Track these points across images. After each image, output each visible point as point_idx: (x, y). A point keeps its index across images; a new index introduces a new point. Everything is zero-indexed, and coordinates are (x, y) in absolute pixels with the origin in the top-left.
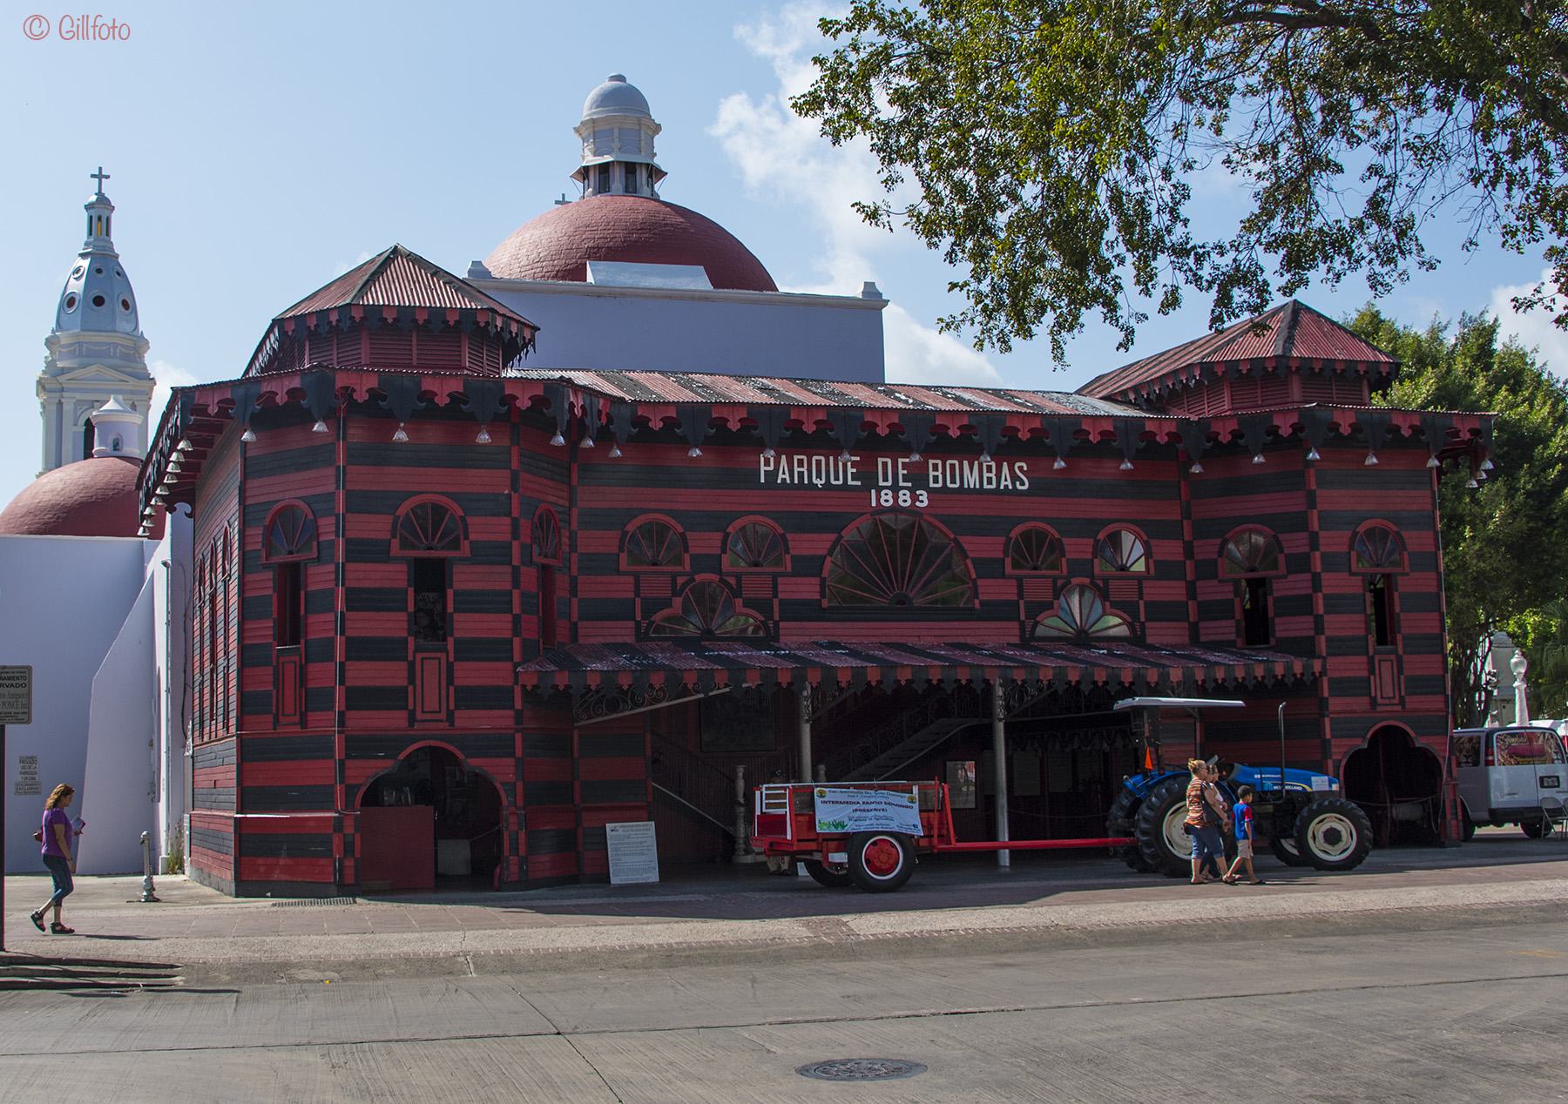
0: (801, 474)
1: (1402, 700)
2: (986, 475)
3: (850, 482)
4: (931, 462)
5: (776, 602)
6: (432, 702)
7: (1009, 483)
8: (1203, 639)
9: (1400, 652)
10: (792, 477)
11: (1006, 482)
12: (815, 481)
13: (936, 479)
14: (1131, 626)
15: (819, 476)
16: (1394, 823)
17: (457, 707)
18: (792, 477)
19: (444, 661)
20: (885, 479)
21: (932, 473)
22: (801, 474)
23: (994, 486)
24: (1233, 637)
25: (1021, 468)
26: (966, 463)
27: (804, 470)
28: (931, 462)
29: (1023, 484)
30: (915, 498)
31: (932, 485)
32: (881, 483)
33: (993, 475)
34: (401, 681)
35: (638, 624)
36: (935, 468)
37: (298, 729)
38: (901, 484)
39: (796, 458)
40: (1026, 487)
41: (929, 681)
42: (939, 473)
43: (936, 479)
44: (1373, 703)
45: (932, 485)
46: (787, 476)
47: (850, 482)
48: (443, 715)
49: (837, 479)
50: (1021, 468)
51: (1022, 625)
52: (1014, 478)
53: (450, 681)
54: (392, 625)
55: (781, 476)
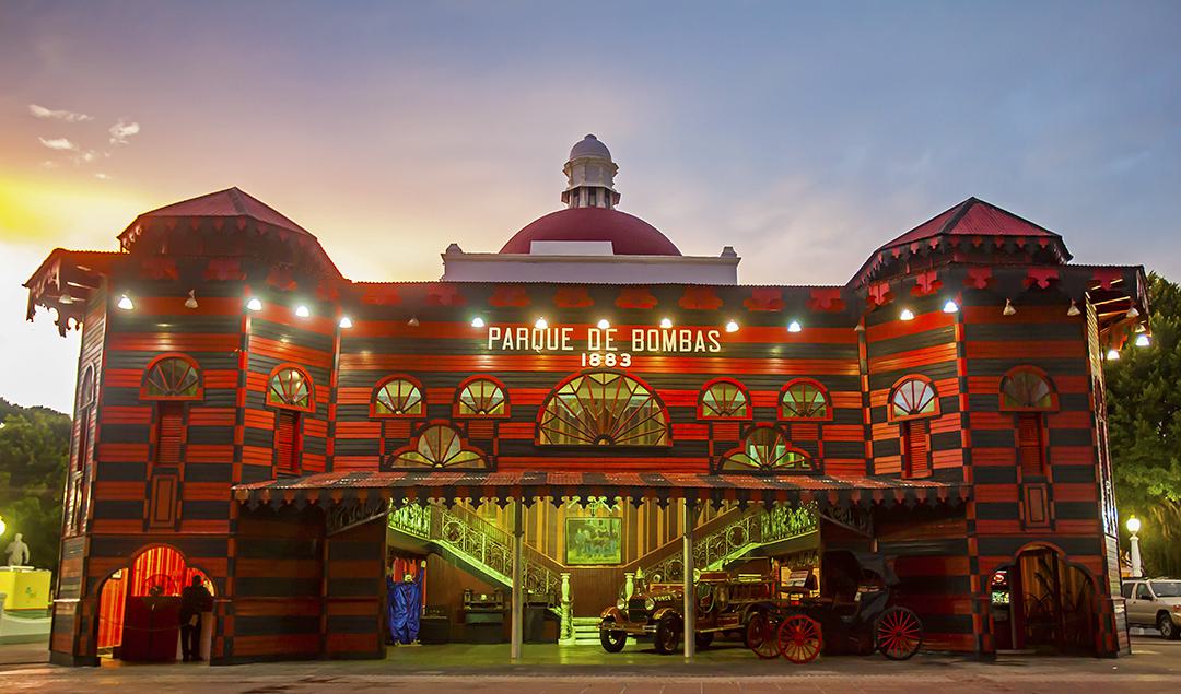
0: (522, 342)
1: (1052, 522)
2: (682, 341)
3: (564, 348)
4: (634, 331)
5: (496, 441)
6: (163, 514)
8: (877, 473)
9: (1051, 481)
11: (700, 346)
13: (638, 345)
14: (485, 459)
15: (537, 344)
16: (995, 623)
17: (1057, 517)
19: (175, 480)
21: (635, 340)
22: (522, 342)
23: (689, 349)
24: (899, 470)
25: (713, 335)
27: (526, 339)
28: (634, 331)
30: (619, 360)
31: (634, 349)
32: (590, 348)
33: (689, 341)
34: (1012, 499)
35: (382, 458)
36: (638, 335)
37: (1050, 531)
39: (519, 330)
41: (261, 502)
42: (641, 340)
43: (638, 345)
44: (1023, 525)
45: (634, 349)
46: (511, 344)
47: (564, 348)
48: (171, 524)
49: (553, 345)
50: (713, 335)
51: (711, 459)
52: (707, 342)
53: (180, 494)
54: (1003, 456)
55: (505, 344)
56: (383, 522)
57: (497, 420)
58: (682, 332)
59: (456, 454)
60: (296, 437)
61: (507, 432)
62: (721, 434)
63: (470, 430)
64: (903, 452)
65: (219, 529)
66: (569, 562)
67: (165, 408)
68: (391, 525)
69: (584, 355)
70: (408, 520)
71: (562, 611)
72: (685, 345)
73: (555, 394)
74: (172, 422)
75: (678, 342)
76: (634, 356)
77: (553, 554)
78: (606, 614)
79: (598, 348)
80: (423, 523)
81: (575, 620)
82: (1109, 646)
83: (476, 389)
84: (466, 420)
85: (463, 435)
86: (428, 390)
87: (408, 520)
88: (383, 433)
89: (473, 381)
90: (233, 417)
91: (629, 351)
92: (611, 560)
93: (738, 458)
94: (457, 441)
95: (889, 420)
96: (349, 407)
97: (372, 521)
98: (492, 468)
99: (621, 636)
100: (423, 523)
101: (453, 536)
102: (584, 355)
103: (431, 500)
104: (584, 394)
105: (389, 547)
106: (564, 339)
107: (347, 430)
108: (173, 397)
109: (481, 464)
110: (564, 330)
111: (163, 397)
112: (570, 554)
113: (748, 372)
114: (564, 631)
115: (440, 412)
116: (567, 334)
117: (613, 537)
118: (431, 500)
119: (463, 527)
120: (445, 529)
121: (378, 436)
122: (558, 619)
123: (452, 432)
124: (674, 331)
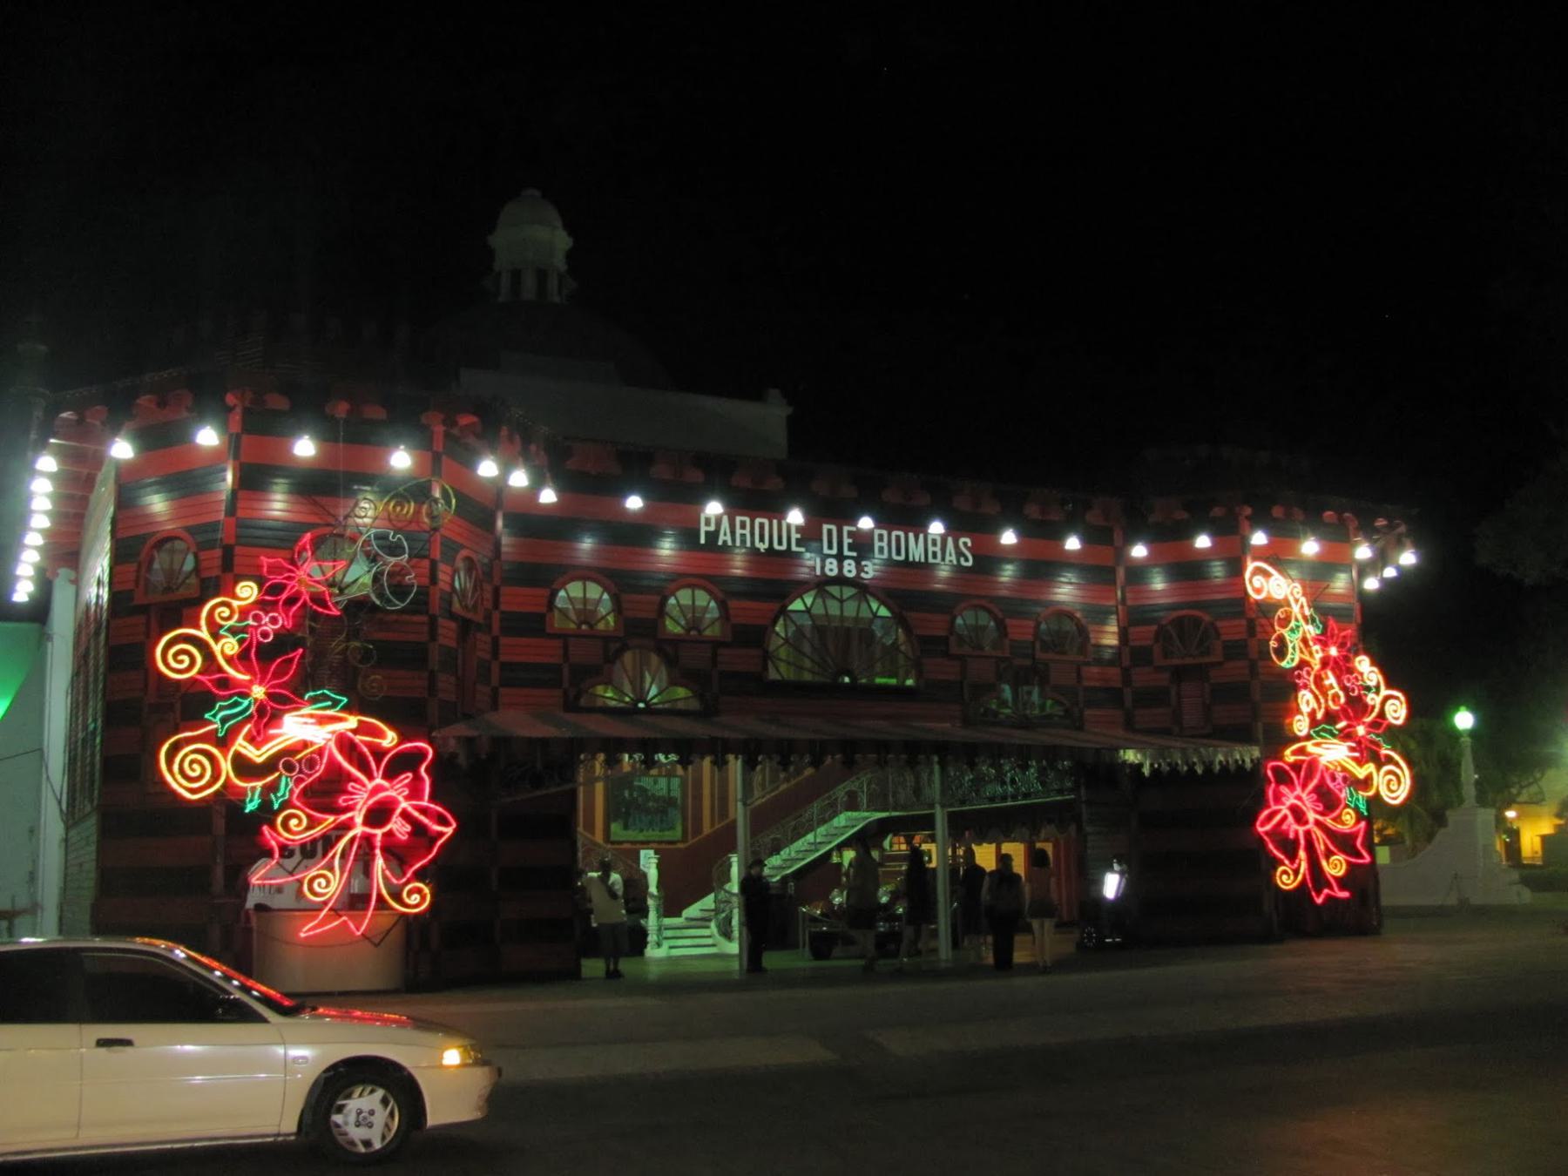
7: (954, 558)
10: (734, 540)
12: (758, 544)
18: (734, 540)
20: (830, 547)
22: (743, 536)
26: (911, 535)
29: (967, 560)
32: (826, 551)
35: (565, 693)
38: (846, 553)
40: (970, 564)
42: (885, 544)
57: (716, 644)
58: (738, 519)
63: (675, 655)
66: (613, 838)
73: (783, 611)
75: (733, 533)
79: (834, 551)
81: (668, 921)
83: (575, 589)
84: (676, 641)
85: (671, 661)
89: (573, 579)
90: (426, 629)
98: (707, 712)
104: (818, 610)
106: (847, 541)
109: (694, 705)
112: (616, 828)
114: (652, 938)
124: (950, 540)
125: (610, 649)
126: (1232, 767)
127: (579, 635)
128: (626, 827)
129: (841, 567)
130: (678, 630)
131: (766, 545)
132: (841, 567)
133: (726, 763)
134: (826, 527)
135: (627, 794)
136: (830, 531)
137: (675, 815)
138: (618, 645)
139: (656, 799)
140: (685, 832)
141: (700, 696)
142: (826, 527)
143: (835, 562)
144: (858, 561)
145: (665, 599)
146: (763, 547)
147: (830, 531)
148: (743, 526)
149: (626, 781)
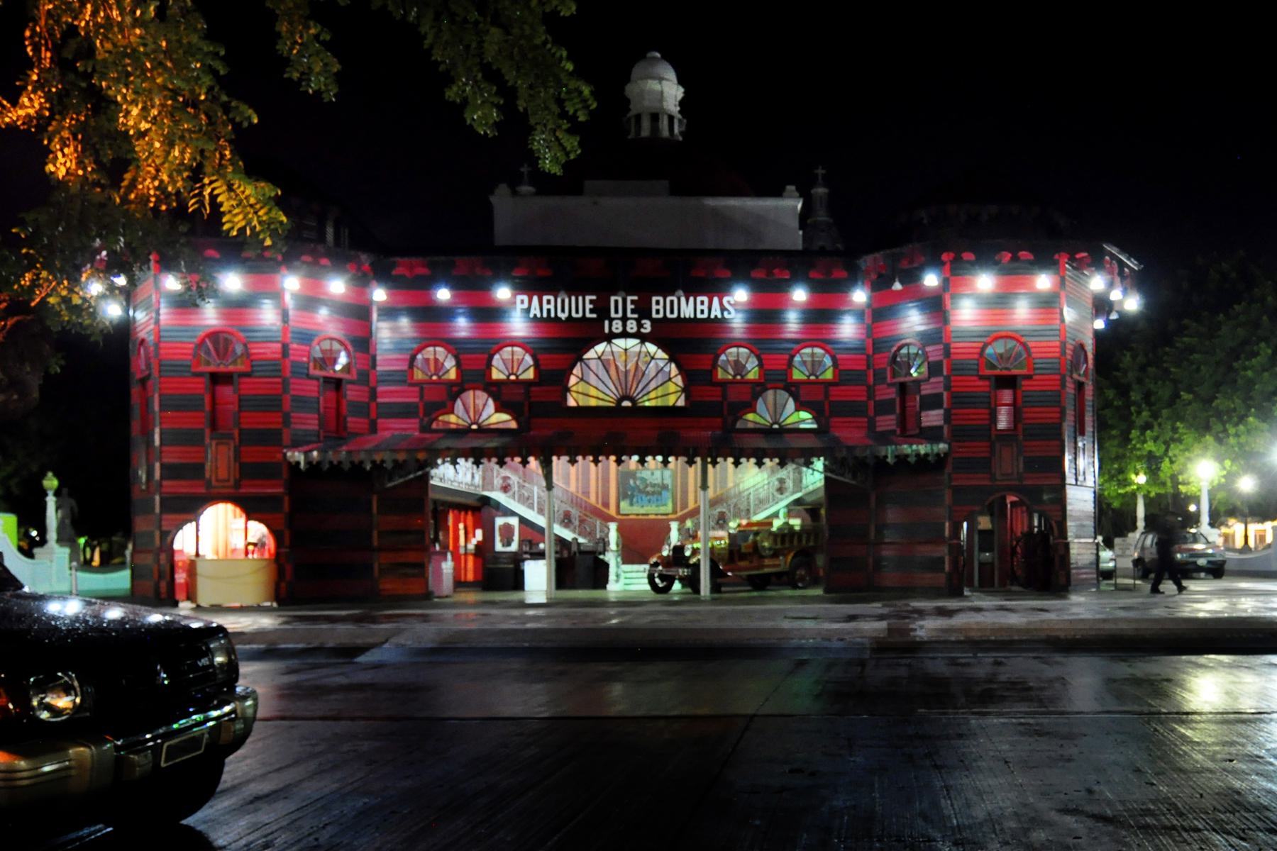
0: (549, 311)
3: (588, 315)
4: (654, 299)
11: (716, 312)
12: (560, 314)
13: (658, 312)
20: (616, 312)
21: (654, 307)
22: (549, 311)
30: (640, 326)
31: (654, 315)
32: (613, 315)
35: (422, 420)
36: (658, 303)
38: (629, 315)
43: (658, 312)
45: (654, 315)
52: (723, 309)
56: (426, 477)
59: (496, 418)
60: (339, 402)
61: (837, 394)
62: (733, 396)
63: (503, 395)
64: (898, 411)
65: (275, 489)
67: (217, 379)
68: (434, 482)
69: (607, 323)
70: (454, 476)
71: (611, 558)
72: (702, 312)
74: (227, 392)
76: (654, 321)
77: (606, 505)
78: (653, 560)
79: (620, 315)
80: (473, 477)
82: (1062, 581)
84: (800, 383)
86: (461, 357)
87: (454, 476)
88: (421, 397)
91: (649, 317)
92: (662, 510)
93: (750, 416)
94: (491, 402)
95: (889, 380)
96: (390, 373)
97: (411, 480)
99: (669, 580)
100: (473, 477)
101: (505, 489)
102: (607, 323)
103: (767, 460)
105: (435, 502)
106: (630, 307)
107: (389, 394)
108: (222, 368)
110: (629, 298)
111: (212, 368)
113: (764, 336)
114: (612, 577)
115: (474, 373)
116: (633, 302)
117: (665, 487)
118: (767, 460)
119: (514, 479)
120: (498, 482)
121: (416, 400)
122: (607, 565)
123: (485, 395)
125: (758, 388)
126: (347, 466)
127: (733, 382)
128: (631, 504)
129: (624, 326)
130: (502, 377)
131: (566, 314)
132: (624, 326)
133: (551, 462)
134: (613, 299)
135: (631, 482)
136: (616, 302)
137: (667, 495)
138: (664, 386)
139: (654, 485)
140: (675, 504)
141: (816, 419)
142: (613, 299)
143: (620, 323)
144: (638, 321)
145: (793, 357)
146: (563, 316)
147: (616, 302)
148: (549, 302)
149: (633, 475)
